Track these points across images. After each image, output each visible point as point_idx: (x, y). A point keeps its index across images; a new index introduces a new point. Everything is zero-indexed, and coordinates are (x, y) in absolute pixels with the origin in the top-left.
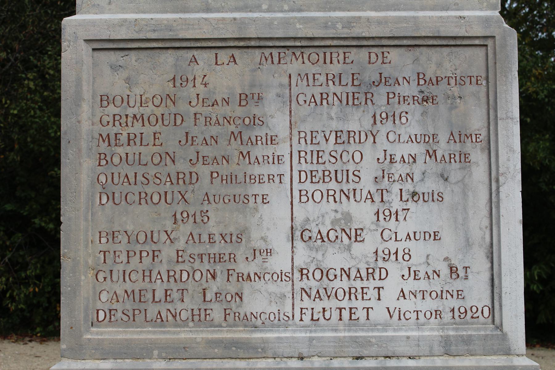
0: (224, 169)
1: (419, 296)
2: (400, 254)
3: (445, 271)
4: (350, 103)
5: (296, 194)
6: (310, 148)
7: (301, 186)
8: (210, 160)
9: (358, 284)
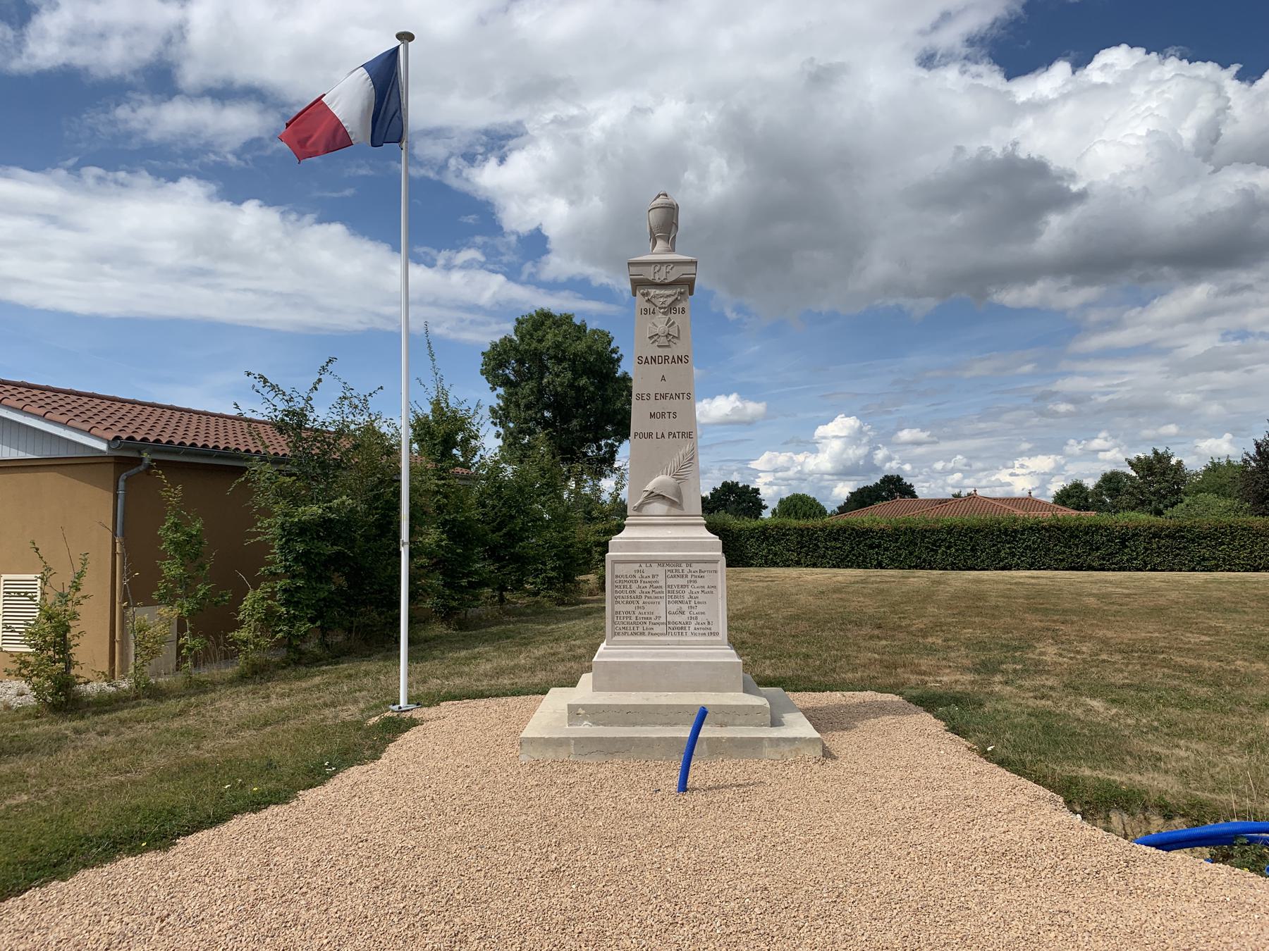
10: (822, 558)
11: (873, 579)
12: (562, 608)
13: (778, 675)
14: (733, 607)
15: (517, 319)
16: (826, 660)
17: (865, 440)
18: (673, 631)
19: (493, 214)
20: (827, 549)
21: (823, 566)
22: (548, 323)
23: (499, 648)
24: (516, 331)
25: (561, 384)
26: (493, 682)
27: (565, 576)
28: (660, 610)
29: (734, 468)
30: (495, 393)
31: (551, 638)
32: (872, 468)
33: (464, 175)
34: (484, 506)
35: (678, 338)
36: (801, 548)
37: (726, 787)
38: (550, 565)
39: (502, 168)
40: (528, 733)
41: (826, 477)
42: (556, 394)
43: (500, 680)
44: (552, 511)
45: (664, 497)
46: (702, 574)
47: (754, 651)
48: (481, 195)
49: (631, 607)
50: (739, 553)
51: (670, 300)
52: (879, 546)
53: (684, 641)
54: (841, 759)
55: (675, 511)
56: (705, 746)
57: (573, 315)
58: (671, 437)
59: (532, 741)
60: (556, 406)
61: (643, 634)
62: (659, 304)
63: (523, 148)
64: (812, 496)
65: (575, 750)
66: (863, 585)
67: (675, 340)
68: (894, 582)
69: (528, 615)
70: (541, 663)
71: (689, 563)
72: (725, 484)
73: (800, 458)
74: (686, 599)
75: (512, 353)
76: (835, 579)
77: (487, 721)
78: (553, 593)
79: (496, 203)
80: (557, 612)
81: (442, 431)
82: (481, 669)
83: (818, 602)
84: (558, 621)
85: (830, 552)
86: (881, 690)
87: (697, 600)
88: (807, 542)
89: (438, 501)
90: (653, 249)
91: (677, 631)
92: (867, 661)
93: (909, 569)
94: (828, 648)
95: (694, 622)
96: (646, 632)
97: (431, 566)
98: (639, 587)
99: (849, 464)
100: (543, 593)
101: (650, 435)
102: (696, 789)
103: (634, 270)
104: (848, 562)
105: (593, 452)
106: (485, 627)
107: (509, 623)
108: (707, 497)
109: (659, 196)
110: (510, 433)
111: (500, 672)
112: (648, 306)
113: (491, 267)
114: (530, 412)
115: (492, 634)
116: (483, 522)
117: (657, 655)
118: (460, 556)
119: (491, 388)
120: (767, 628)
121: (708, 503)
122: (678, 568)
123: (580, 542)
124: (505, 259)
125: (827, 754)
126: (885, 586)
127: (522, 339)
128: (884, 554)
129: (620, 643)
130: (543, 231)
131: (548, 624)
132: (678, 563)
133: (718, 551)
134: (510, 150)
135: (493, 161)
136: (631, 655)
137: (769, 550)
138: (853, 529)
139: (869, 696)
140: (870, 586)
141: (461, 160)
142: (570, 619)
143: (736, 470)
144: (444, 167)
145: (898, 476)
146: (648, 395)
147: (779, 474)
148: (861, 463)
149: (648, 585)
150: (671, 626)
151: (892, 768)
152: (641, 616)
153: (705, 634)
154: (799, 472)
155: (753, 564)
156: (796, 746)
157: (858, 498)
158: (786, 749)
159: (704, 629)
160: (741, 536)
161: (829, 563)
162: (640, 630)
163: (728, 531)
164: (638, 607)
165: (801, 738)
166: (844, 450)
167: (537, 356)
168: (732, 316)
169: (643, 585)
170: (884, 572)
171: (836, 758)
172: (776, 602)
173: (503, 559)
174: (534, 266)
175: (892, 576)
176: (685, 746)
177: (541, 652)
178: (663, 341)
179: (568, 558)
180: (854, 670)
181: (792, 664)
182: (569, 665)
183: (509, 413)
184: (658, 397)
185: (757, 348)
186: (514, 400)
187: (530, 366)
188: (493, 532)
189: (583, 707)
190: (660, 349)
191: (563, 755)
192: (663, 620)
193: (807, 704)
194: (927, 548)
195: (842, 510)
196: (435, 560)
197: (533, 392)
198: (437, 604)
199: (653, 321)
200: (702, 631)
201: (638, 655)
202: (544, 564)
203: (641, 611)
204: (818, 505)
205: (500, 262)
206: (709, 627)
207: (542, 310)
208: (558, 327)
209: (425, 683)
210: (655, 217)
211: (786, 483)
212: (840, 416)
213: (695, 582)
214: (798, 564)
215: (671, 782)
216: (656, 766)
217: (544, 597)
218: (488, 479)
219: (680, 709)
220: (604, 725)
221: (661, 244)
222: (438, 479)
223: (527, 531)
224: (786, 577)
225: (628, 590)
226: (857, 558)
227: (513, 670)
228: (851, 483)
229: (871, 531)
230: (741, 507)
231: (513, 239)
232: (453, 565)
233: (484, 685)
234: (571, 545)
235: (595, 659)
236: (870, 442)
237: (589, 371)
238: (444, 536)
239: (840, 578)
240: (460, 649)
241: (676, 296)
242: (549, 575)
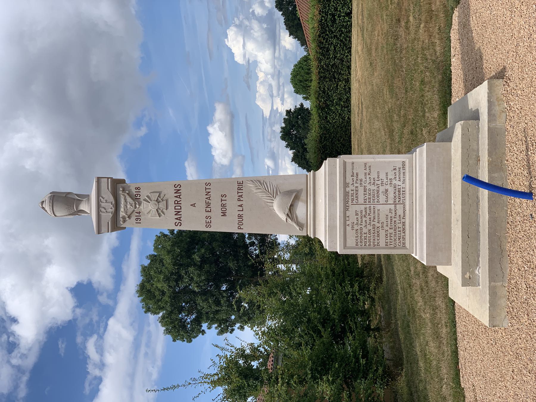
0: (372, 219)
1: (400, 177)
2: (391, 181)
3: (395, 171)
4: (242, 185)
5: (373, 203)
6: (368, 201)
7: (376, 202)
8: (370, 222)
9: (397, 190)
10: (343, 61)
11: (360, 22)
12: (385, 279)
13: (437, 107)
14: (383, 138)
15: (146, 312)
16: (426, 67)
17: (247, 23)
18: (402, 198)
19: (58, 328)
20: (335, 57)
21: (349, 61)
22: (148, 286)
23: (417, 334)
24: (155, 313)
25: (199, 276)
26: (445, 343)
27: (358, 276)
28: (384, 209)
29: (269, 130)
30: (207, 330)
31: (408, 290)
32: (269, 17)
33: (25, 352)
34: (300, 344)
35: (160, 193)
36: (335, 78)
37: (528, 160)
38: (348, 289)
39: (20, 320)
40: (486, 321)
41: (277, 54)
42: (208, 280)
43: (443, 336)
44: (304, 286)
45: (292, 205)
46: (355, 175)
47: (418, 125)
48: (43, 338)
49: (382, 233)
50: (339, 129)
51: (129, 199)
52: (333, 15)
53: (410, 190)
54: (505, 64)
55: (303, 196)
56: (496, 175)
57: (141, 266)
58: (241, 199)
59: (492, 317)
60: (217, 281)
61: (404, 224)
62: (132, 208)
63: (4, 303)
64: (293, 68)
65: (499, 282)
66: (365, 30)
67: (162, 195)
68: (362, 5)
69: (390, 307)
70: (430, 300)
71: (345, 185)
72: (283, 138)
73: (261, 75)
75: (173, 316)
76: (360, 53)
77: (476, 350)
78: (372, 286)
79: (50, 325)
80: (387, 283)
81: (237, 379)
82: (434, 350)
83: (379, 68)
84: (395, 283)
85: (338, 55)
86: (449, 25)
87: (376, 179)
88: (330, 74)
89: (295, 382)
90: (86, 213)
91: (401, 195)
92: (426, 34)
94: (416, 64)
95: (394, 182)
96: (403, 220)
97: (349, 388)
98: (366, 226)
99: (266, 36)
100: (372, 294)
101: (240, 216)
102: (530, 184)
103: (104, 228)
104: (346, 40)
105: (255, 250)
106: (400, 344)
107: (396, 324)
108: (294, 153)
109: (43, 208)
110: (240, 318)
111: (437, 336)
112: (133, 218)
113: (102, 330)
114: (222, 302)
115: (405, 338)
116: (313, 345)
117: (421, 212)
118: (342, 365)
119: (203, 334)
120: (399, 112)
121: (299, 152)
122: (350, 195)
123: (330, 263)
124: (95, 318)
125: (501, 75)
126: (366, 13)
127: (162, 308)
128: (340, 11)
129: (411, 242)
130: (73, 287)
131: (397, 291)
132: (346, 195)
134: (6, 313)
135: (15, 328)
136: (421, 234)
137: (337, 104)
138: (319, 36)
139: (454, 35)
140: (365, 24)
141: (13, 354)
142: (393, 273)
143: (271, 128)
144: (19, 369)
146: (207, 217)
147: (275, 92)
148: (265, 26)
149: (364, 219)
151: (512, 23)
152: (389, 225)
153: (404, 173)
154: (273, 76)
155: (348, 118)
156: (495, 100)
157: (294, 30)
158: (497, 109)
159: (400, 174)
160: (325, 127)
161: (347, 56)
162: (401, 225)
163: (321, 138)
164: (382, 227)
165: (488, 97)
166: (255, 40)
167: (175, 297)
168: (144, 131)
169: (364, 224)
170: (354, 12)
171: (505, 68)
172: (379, 102)
173: (343, 329)
174: (102, 294)
175: (358, 5)
176: (496, 194)
177: (420, 299)
178: (162, 205)
179: (343, 274)
180: (433, 44)
181: (428, 95)
182: (430, 278)
183: (223, 320)
184: (208, 209)
185: (171, 111)
186: (212, 316)
187: (184, 302)
188: (321, 337)
189: (464, 274)
190: (169, 208)
191: (504, 292)
192: (392, 207)
193: (461, 86)
195: (303, 43)
196: (344, 386)
197: (206, 300)
198: (381, 384)
199: (146, 213)
200: (402, 175)
201: (421, 229)
202: (347, 294)
203: (385, 225)
204: (300, 62)
205: (98, 322)
206: (398, 169)
207: (137, 291)
208: (152, 278)
209: (445, 398)
210: (60, 212)
211: (281, 88)
212: (227, 43)
213: (361, 180)
214: (348, 81)
215: (524, 204)
216: (512, 215)
217: (375, 294)
218: (277, 341)
219: (465, 194)
220: (478, 256)
221: (83, 207)
222: (277, 384)
223: (320, 309)
224: (359, 92)
225: (368, 235)
226: (343, 33)
227: (435, 325)
228: (281, 34)
230: (301, 125)
231: (78, 311)
232: (349, 371)
233: (447, 349)
234: (333, 271)
235: (425, 263)
236: (248, 18)
237: (188, 252)
238: (325, 378)
239: (359, 48)
240: (418, 367)
241: (126, 194)
242: (357, 290)
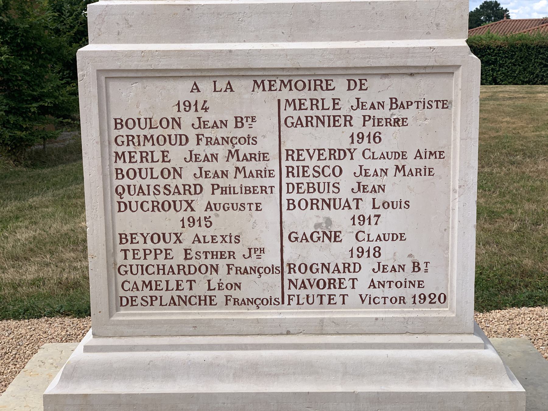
18: (303, 293)
46: (399, 114)
53: (334, 322)
74: (345, 194)
87: (380, 197)
91: (315, 291)
93: (522, 84)
96: (220, 296)
98: (193, 157)
122: (318, 94)
128: (499, 71)
133: (451, 33)
145: (496, 2)
149: (221, 150)
150: (298, 276)
152: (202, 247)
153: (402, 300)
159: (399, 284)
162: (200, 289)
164: (192, 221)
169: (203, 150)
194: (541, 63)
200: (394, 292)
203: (202, 231)
213: (376, 138)
225: (157, 168)
229: (488, 47)
